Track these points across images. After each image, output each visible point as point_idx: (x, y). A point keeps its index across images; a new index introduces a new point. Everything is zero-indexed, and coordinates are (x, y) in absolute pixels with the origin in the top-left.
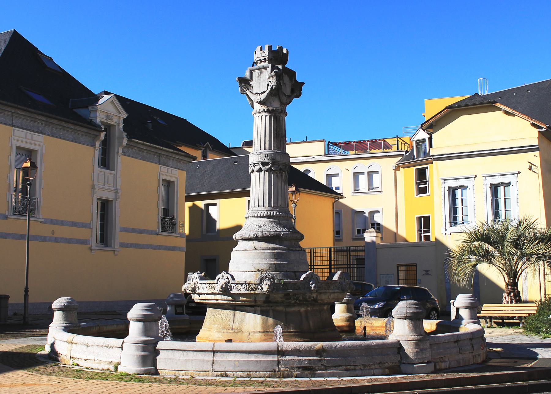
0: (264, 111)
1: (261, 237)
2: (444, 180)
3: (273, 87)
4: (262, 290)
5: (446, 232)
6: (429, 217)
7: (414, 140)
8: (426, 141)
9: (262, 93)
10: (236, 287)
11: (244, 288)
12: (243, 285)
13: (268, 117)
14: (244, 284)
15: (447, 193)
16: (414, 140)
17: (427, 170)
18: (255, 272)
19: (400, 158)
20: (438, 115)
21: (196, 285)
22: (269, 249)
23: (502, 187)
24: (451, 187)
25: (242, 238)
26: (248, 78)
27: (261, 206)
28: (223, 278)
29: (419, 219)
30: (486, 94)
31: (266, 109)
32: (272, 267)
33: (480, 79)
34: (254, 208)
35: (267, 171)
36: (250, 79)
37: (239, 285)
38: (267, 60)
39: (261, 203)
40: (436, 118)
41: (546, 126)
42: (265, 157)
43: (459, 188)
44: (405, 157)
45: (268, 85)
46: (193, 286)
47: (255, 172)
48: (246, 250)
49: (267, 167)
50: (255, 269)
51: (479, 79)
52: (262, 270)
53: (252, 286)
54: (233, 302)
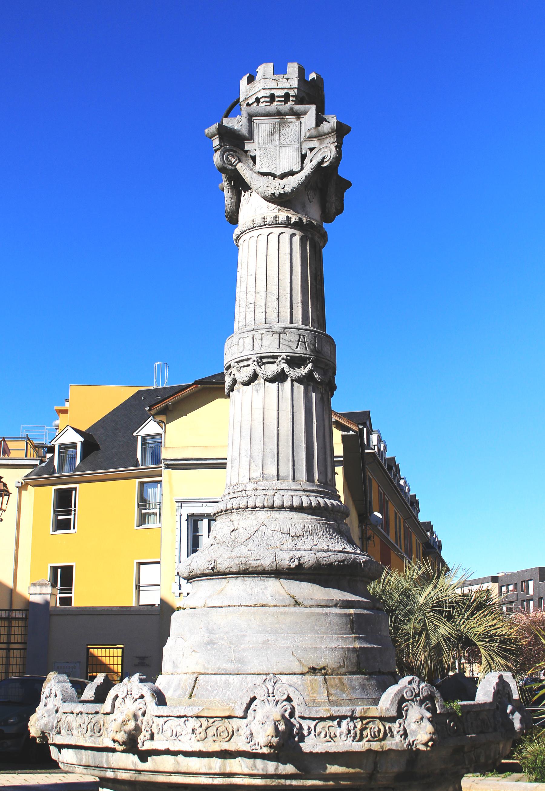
0: (287, 224)
1: (310, 568)
2: (182, 503)
3: (322, 161)
4: (405, 739)
5: (180, 591)
6: (71, 567)
7: (56, 443)
8: (76, 447)
9: (283, 176)
10: (318, 729)
11: (349, 731)
12: (344, 723)
13: (297, 240)
14: (349, 719)
15: (185, 524)
16: (56, 443)
17: (74, 492)
18: (302, 674)
19: (29, 471)
20: (180, 394)
21: (139, 722)
22: (336, 606)
23: (206, 521)
24: (193, 515)
25: (242, 568)
26: (244, 131)
27: (286, 478)
28: (271, 699)
29: (55, 569)
30: (165, 386)
31: (294, 219)
32: (349, 659)
33: (158, 363)
34: (263, 483)
35: (299, 380)
36: (247, 135)
37: (330, 723)
38: (291, 99)
39: (286, 470)
40: (176, 398)
41: (358, 427)
42: (299, 341)
43: (205, 518)
44: (39, 469)
45: (303, 157)
46: (131, 725)
47: (260, 381)
48: (263, 606)
49: (302, 371)
50: (303, 665)
51: (156, 363)
52: (324, 668)
53: (371, 725)
54: (295, 783)
